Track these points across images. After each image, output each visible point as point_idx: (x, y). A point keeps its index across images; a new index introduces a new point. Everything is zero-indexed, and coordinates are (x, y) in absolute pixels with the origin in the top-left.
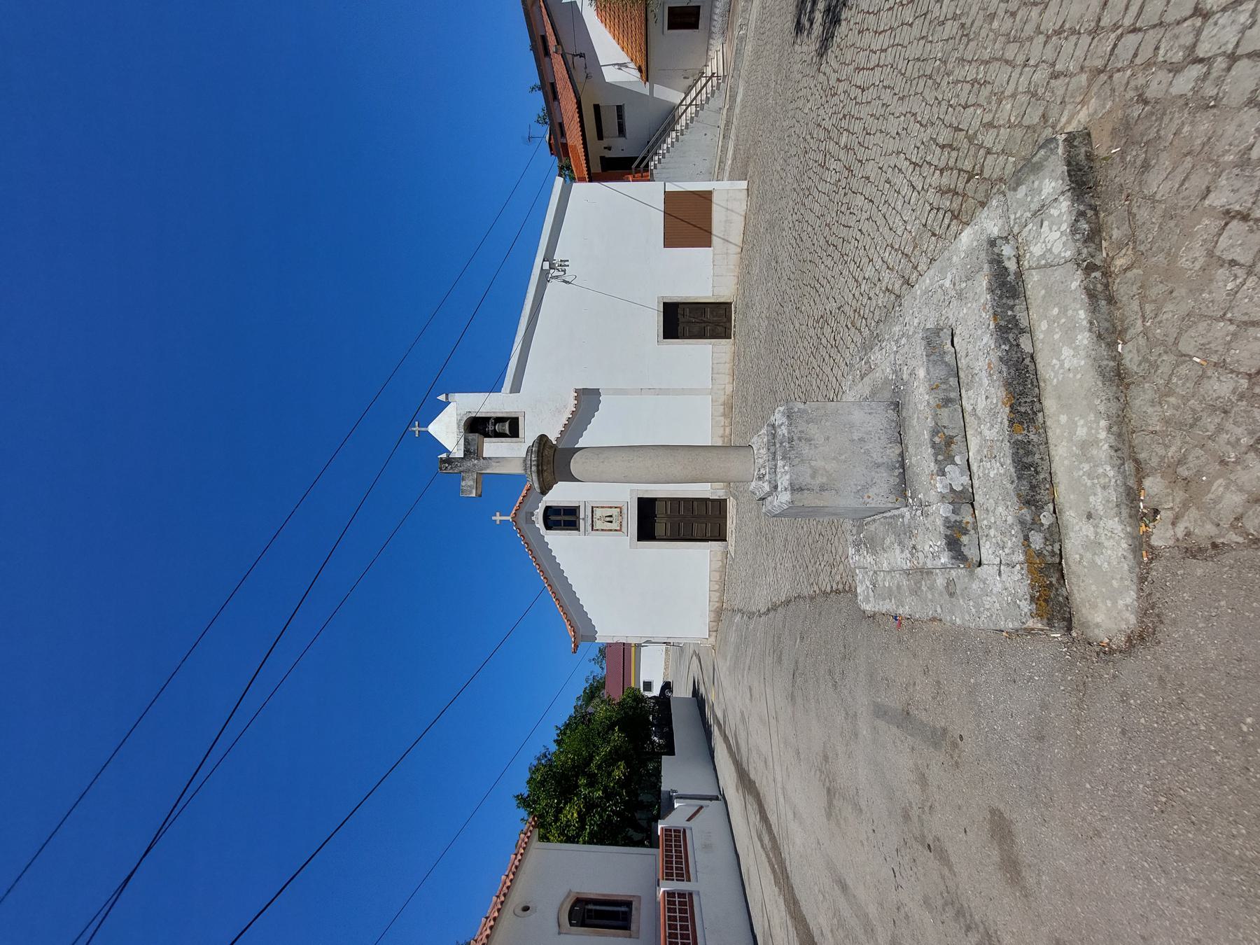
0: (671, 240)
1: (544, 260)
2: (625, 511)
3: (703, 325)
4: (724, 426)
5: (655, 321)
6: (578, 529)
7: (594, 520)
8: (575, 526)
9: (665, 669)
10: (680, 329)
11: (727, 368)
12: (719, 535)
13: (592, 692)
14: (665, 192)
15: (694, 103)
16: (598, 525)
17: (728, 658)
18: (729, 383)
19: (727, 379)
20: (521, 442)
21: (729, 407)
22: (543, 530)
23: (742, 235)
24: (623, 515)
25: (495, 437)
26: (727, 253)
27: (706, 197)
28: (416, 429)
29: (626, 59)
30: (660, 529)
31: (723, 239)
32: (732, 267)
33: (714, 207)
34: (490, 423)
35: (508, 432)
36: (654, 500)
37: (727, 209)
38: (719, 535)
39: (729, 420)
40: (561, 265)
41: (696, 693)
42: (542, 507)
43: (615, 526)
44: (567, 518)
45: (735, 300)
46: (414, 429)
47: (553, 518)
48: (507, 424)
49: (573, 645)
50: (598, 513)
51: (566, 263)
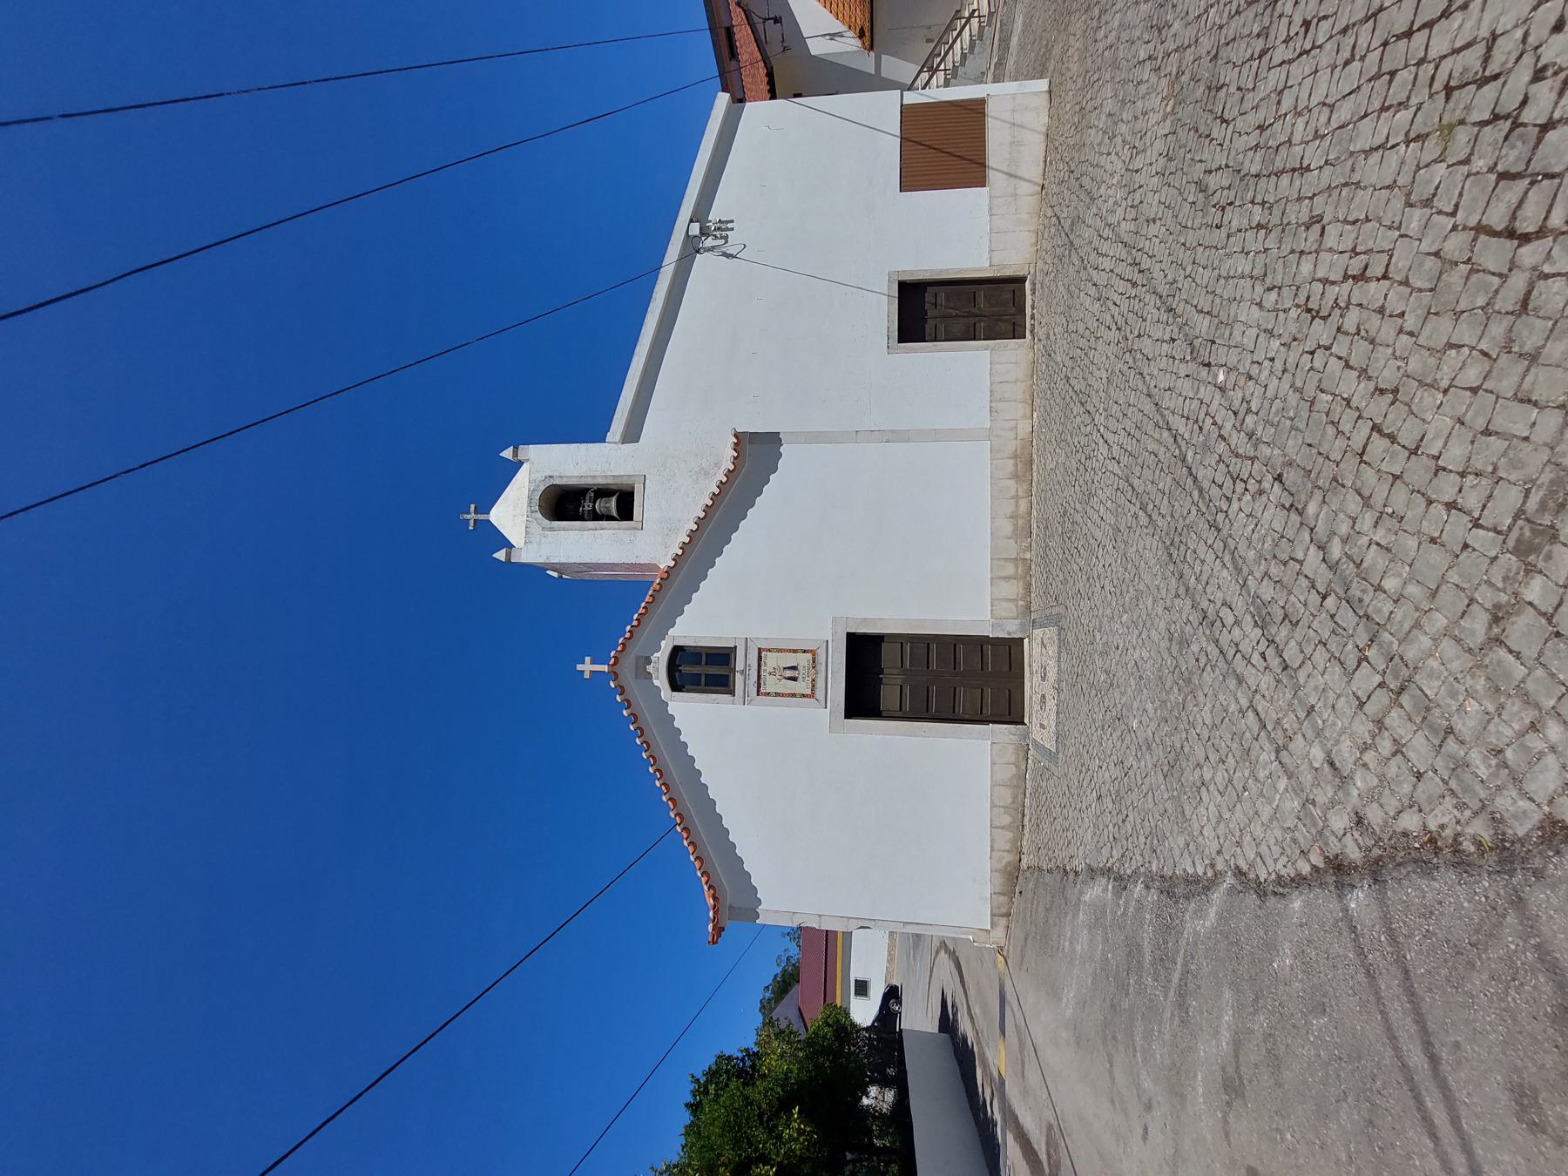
0: (911, 180)
1: (691, 221)
2: (821, 658)
3: (972, 320)
4: (1016, 498)
5: (883, 312)
6: (732, 693)
7: (763, 674)
8: (727, 685)
9: (888, 961)
10: (929, 326)
11: (1019, 391)
12: (1010, 711)
13: (784, 981)
14: (902, 106)
15: (942, 67)
16: (771, 684)
17: (1069, 995)
18: (1024, 417)
19: (1021, 410)
20: (635, 529)
21: (1025, 462)
22: (665, 691)
23: (1042, 165)
24: (818, 667)
25: (594, 519)
26: (1016, 194)
27: (976, 109)
28: (471, 516)
29: (838, 26)
30: (889, 696)
31: (1006, 173)
32: (1025, 216)
33: (991, 123)
34: (587, 498)
35: (614, 513)
36: (879, 639)
37: (1014, 124)
38: (1010, 711)
39: (1025, 486)
40: (719, 229)
41: (947, 1024)
42: (666, 647)
43: (802, 687)
44: (714, 670)
45: (1032, 271)
46: (468, 517)
47: (686, 669)
48: (614, 500)
49: (710, 927)
50: (771, 661)
51: (729, 225)
